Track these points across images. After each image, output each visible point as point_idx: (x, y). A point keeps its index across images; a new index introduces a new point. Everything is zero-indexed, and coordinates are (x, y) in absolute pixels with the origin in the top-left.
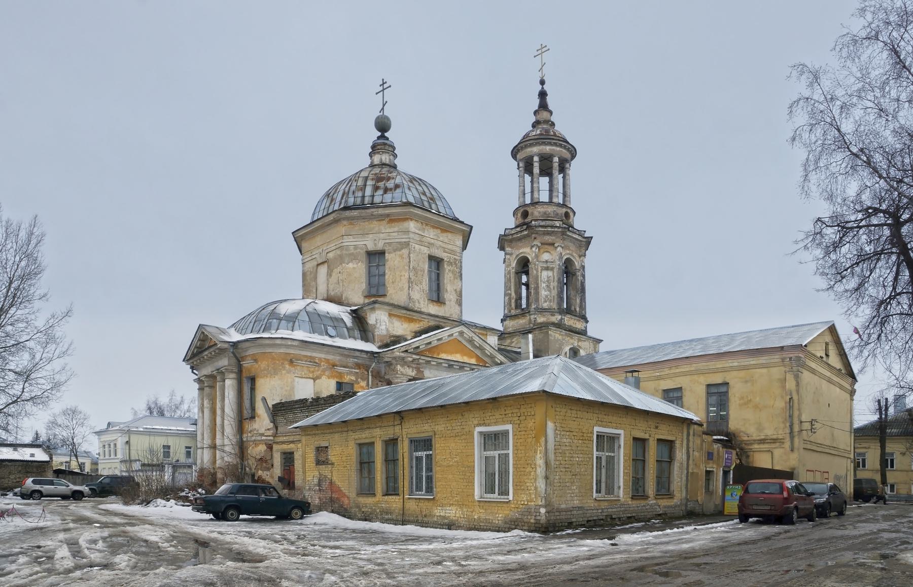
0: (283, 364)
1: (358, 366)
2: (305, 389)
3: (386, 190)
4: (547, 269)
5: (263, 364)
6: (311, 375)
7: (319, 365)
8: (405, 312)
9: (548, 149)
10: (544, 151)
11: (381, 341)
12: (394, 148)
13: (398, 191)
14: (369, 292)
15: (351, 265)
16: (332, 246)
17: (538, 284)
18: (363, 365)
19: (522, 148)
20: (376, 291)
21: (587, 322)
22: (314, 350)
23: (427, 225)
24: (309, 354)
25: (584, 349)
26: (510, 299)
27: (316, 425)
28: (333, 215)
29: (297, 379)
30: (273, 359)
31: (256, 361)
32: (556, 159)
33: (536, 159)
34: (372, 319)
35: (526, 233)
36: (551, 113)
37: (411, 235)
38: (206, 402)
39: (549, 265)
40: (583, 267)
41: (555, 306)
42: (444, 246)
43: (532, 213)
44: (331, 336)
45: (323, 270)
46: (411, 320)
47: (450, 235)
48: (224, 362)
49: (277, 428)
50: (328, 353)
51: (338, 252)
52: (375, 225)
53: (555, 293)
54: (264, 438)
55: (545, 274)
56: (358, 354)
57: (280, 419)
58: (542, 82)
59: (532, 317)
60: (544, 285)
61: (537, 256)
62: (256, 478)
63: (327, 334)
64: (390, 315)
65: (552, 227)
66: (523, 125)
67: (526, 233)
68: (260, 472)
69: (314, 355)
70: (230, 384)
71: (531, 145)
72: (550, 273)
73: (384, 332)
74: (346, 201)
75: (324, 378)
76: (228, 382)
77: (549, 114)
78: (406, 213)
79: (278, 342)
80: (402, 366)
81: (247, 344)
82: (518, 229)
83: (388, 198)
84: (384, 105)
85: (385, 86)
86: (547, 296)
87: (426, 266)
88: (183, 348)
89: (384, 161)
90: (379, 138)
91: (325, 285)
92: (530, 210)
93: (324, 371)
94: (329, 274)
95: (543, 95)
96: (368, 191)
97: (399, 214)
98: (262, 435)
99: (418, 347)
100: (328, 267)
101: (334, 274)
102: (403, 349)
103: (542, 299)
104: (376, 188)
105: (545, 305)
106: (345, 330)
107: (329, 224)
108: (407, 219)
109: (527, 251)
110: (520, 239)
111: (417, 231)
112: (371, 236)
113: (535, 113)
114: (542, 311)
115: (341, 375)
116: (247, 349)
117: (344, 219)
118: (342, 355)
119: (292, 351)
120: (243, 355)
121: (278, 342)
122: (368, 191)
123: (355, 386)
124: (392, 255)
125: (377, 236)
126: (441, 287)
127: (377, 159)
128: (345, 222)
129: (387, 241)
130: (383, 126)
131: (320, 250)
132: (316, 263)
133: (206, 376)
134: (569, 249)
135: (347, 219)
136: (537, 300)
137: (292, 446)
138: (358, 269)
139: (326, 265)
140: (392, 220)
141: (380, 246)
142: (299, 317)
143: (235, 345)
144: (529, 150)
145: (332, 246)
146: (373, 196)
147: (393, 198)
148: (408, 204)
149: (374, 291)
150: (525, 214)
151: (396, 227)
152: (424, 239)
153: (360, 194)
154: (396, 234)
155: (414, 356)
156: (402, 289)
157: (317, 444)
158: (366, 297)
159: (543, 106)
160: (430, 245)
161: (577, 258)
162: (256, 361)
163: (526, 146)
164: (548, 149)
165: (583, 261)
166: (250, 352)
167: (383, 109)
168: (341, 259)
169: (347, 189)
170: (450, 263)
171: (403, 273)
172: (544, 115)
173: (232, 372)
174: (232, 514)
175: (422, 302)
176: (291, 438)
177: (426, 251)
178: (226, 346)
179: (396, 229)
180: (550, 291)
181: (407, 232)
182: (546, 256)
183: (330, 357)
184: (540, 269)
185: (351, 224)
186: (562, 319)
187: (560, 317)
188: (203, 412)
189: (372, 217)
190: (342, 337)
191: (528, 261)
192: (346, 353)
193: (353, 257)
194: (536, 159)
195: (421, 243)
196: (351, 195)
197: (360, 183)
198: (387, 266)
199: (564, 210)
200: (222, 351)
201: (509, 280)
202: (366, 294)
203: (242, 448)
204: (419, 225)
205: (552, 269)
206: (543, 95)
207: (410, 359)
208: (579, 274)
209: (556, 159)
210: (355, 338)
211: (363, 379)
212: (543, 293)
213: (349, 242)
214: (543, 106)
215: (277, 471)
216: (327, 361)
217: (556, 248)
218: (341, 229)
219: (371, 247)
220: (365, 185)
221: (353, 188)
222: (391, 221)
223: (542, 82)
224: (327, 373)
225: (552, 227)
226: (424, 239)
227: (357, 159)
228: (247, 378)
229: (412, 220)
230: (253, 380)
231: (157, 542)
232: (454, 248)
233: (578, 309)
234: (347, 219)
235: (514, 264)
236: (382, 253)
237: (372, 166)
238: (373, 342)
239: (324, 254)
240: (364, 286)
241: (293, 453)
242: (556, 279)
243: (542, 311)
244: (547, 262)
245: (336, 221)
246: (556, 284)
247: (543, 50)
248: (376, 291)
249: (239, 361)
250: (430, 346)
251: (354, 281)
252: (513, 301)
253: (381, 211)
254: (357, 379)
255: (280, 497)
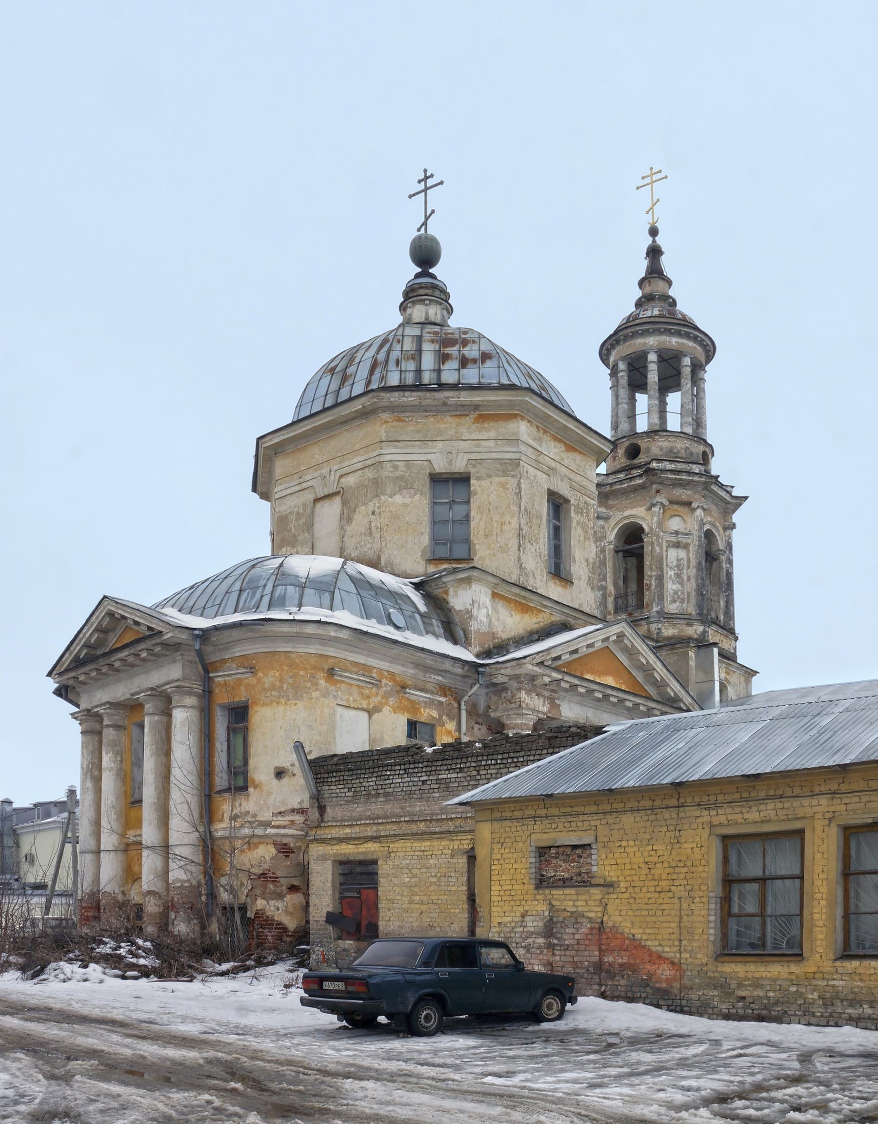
0: (313, 676)
1: (443, 690)
2: (352, 734)
3: (464, 362)
4: (677, 545)
5: (269, 678)
6: (364, 704)
7: (377, 684)
8: (517, 591)
9: (674, 341)
10: (668, 346)
11: (481, 645)
12: (448, 295)
13: (488, 363)
14: (433, 552)
15: (398, 499)
16: (357, 461)
17: (662, 571)
18: (450, 689)
19: (626, 338)
20: (452, 551)
21: (736, 639)
22: (370, 653)
23: (545, 432)
24: (361, 659)
25: (734, 686)
26: (605, 596)
27: (551, 796)
28: (363, 400)
29: (340, 710)
30: (292, 665)
31: (252, 670)
32: (687, 361)
33: (652, 357)
34: (459, 599)
35: (639, 481)
36: (669, 283)
37: (523, 448)
38: (107, 759)
39: (680, 538)
40: (729, 546)
41: (692, 610)
42: (572, 476)
43: (648, 450)
44: (397, 628)
45: (330, 511)
46: (524, 608)
47: (578, 457)
48: (171, 672)
49: (322, 809)
50: (394, 660)
51: (370, 474)
52: (448, 424)
53: (691, 586)
54: (270, 831)
55: (673, 555)
56: (448, 665)
57: (333, 790)
58: (654, 232)
59: (653, 627)
60: (671, 573)
61: (660, 524)
62: (250, 914)
63: (391, 622)
64: (495, 595)
65: (689, 473)
66: (621, 302)
67: (639, 481)
68: (260, 903)
69: (372, 662)
70: (183, 718)
71: (645, 333)
72: (682, 554)
73: (484, 629)
74: (383, 378)
75: (386, 710)
76: (180, 716)
77: (667, 285)
78: (512, 405)
79: (310, 629)
80: (528, 693)
81: (235, 634)
82: (622, 476)
83: (470, 375)
84: (427, 218)
85: (430, 182)
86: (676, 592)
87: (545, 510)
88: (56, 642)
89: (432, 318)
90: (417, 276)
91: (336, 538)
92: (643, 444)
93: (386, 696)
94: (346, 517)
95: (654, 252)
96: (428, 361)
97: (498, 405)
98: (267, 824)
99: (558, 658)
100: (344, 503)
101: (357, 517)
102: (538, 659)
103: (668, 598)
104: (444, 358)
105: (672, 608)
106: (417, 616)
107: (346, 421)
108: (515, 416)
109: (638, 513)
110: (624, 492)
111: (531, 442)
112: (440, 445)
113: (641, 283)
114: (669, 618)
115: (413, 707)
116: (228, 645)
117: (385, 409)
118: (417, 665)
119: (331, 652)
120: (214, 658)
121: (310, 629)
122: (428, 361)
123: (438, 729)
124: (485, 483)
125: (453, 445)
126: (564, 553)
127: (418, 312)
128: (385, 416)
129: (474, 456)
130: (425, 254)
131: (325, 471)
132: (311, 497)
133: (112, 705)
134: (711, 515)
135: (391, 408)
136: (661, 598)
137: (371, 846)
138: (414, 507)
139: (338, 500)
140: (483, 416)
141: (459, 465)
142: (339, 584)
143: (204, 635)
144: (639, 341)
145: (357, 461)
146: (439, 371)
147: (480, 376)
148: (512, 387)
149: (443, 552)
150: (634, 451)
151: (492, 430)
152: (541, 458)
153: (411, 366)
154: (491, 444)
155: (556, 675)
156: (504, 549)
157: (545, 839)
158: (431, 561)
159: (655, 272)
160: (551, 472)
161: (722, 531)
162: (252, 670)
163: (635, 335)
164: (674, 341)
165: (730, 537)
166: (238, 651)
167: (425, 224)
168: (376, 487)
169: (381, 356)
170: (579, 511)
171: (507, 518)
172: (658, 286)
173: (190, 693)
174: (428, 1018)
175: (539, 577)
176: (370, 831)
177: (545, 483)
178: (184, 636)
179: (492, 434)
180: (681, 583)
181: (515, 440)
182: (675, 524)
183: (397, 669)
184: (665, 545)
185: (399, 420)
186: (704, 632)
187: (701, 629)
188: (97, 781)
189: (443, 409)
190: (415, 630)
191: (641, 529)
192: (429, 661)
193: (403, 484)
194: (652, 357)
195: (537, 464)
196: (392, 365)
197: (408, 345)
198: (474, 505)
199: (702, 448)
200: (173, 647)
201: (603, 563)
202: (428, 556)
203: (210, 850)
204: (533, 430)
205: (686, 546)
206: (654, 252)
207: (547, 680)
208: (723, 558)
209: (687, 361)
210: (436, 636)
211: (451, 718)
212: (671, 586)
213: (390, 453)
214: (655, 272)
215: (323, 897)
216: (392, 675)
217: (694, 510)
218: (379, 428)
219: (440, 466)
220: (420, 351)
221: (395, 354)
222: (482, 418)
223: (654, 232)
224: (392, 701)
225: (689, 473)
226: (541, 458)
227: (374, 312)
228: (223, 707)
229: (523, 418)
230: (240, 715)
231: (200, 1094)
232: (585, 483)
233: (722, 618)
234: (391, 408)
235: (612, 536)
236: (463, 480)
237: (407, 322)
238: (467, 644)
239: (334, 477)
240: (426, 540)
241: (375, 862)
242: (693, 562)
243: (669, 618)
244: (677, 533)
245: (366, 414)
246: (693, 572)
247: (653, 177)
248: (452, 551)
249: (207, 669)
250: (559, 663)
251: (406, 525)
252: (611, 600)
253: (465, 397)
254: (441, 716)
255: (517, 965)
